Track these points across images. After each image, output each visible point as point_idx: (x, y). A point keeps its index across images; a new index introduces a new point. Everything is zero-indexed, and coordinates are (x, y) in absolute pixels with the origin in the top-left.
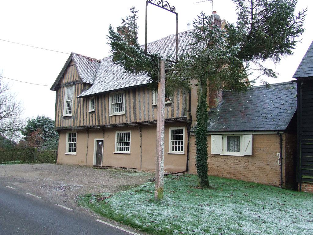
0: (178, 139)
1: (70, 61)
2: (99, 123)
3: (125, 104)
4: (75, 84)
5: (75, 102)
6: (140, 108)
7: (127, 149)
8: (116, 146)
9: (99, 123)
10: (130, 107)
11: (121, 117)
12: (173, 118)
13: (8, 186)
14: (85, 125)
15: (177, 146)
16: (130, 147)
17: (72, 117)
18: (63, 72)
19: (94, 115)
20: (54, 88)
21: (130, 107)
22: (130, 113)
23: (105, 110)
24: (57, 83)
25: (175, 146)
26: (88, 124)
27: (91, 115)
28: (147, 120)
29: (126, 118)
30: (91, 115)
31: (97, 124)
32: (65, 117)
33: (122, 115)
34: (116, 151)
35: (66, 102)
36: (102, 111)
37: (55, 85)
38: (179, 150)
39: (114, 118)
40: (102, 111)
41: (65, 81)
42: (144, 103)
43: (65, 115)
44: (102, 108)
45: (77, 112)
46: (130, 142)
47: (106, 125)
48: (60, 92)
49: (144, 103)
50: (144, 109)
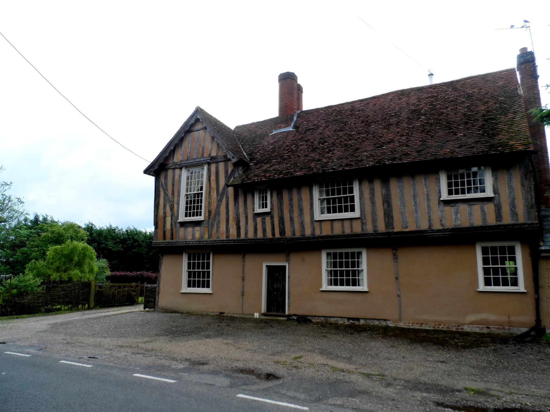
0: (198, 268)
1: (193, 121)
2: (282, 232)
3: (361, 198)
4: (209, 164)
5: (210, 194)
6: (403, 204)
7: (206, 284)
8: (325, 277)
9: (282, 232)
10: (373, 203)
11: (323, 224)
12: (499, 223)
13: (8, 353)
14: (243, 236)
15: (192, 279)
16: (211, 279)
17: (205, 223)
18: (176, 141)
19: (268, 219)
20: (153, 170)
21: (373, 203)
22: (374, 213)
23: (301, 210)
24: (161, 161)
25: (333, 278)
26: (251, 235)
27: (259, 220)
28: (424, 226)
29: (363, 224)
30: (259, 220)
31: (277, 235)
32: (183, 224)
33: (351, 219)
34: (325, 287)
35: (184, 195)
36: (291, 211)
37: (158, 164)
38: (203, 287)
39: (347, 224)
40: (291, 211)
41: (178, 157)
42: (415, 196)
43: (182, 218)
44: (291, 206)
45: (218, 213)
46: (211, 270)
47: (314, 238)
48: (166, 177)
49: (415, 196)
50: (416, 208)
